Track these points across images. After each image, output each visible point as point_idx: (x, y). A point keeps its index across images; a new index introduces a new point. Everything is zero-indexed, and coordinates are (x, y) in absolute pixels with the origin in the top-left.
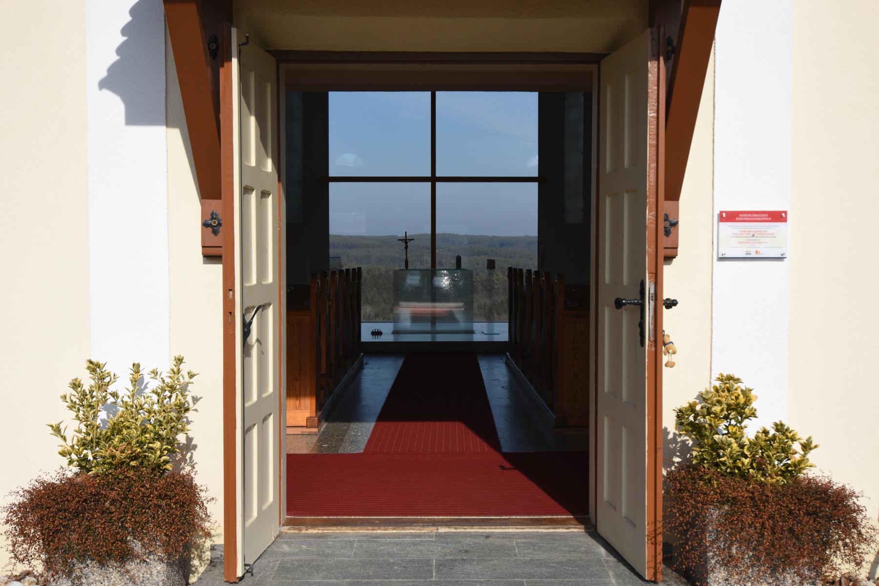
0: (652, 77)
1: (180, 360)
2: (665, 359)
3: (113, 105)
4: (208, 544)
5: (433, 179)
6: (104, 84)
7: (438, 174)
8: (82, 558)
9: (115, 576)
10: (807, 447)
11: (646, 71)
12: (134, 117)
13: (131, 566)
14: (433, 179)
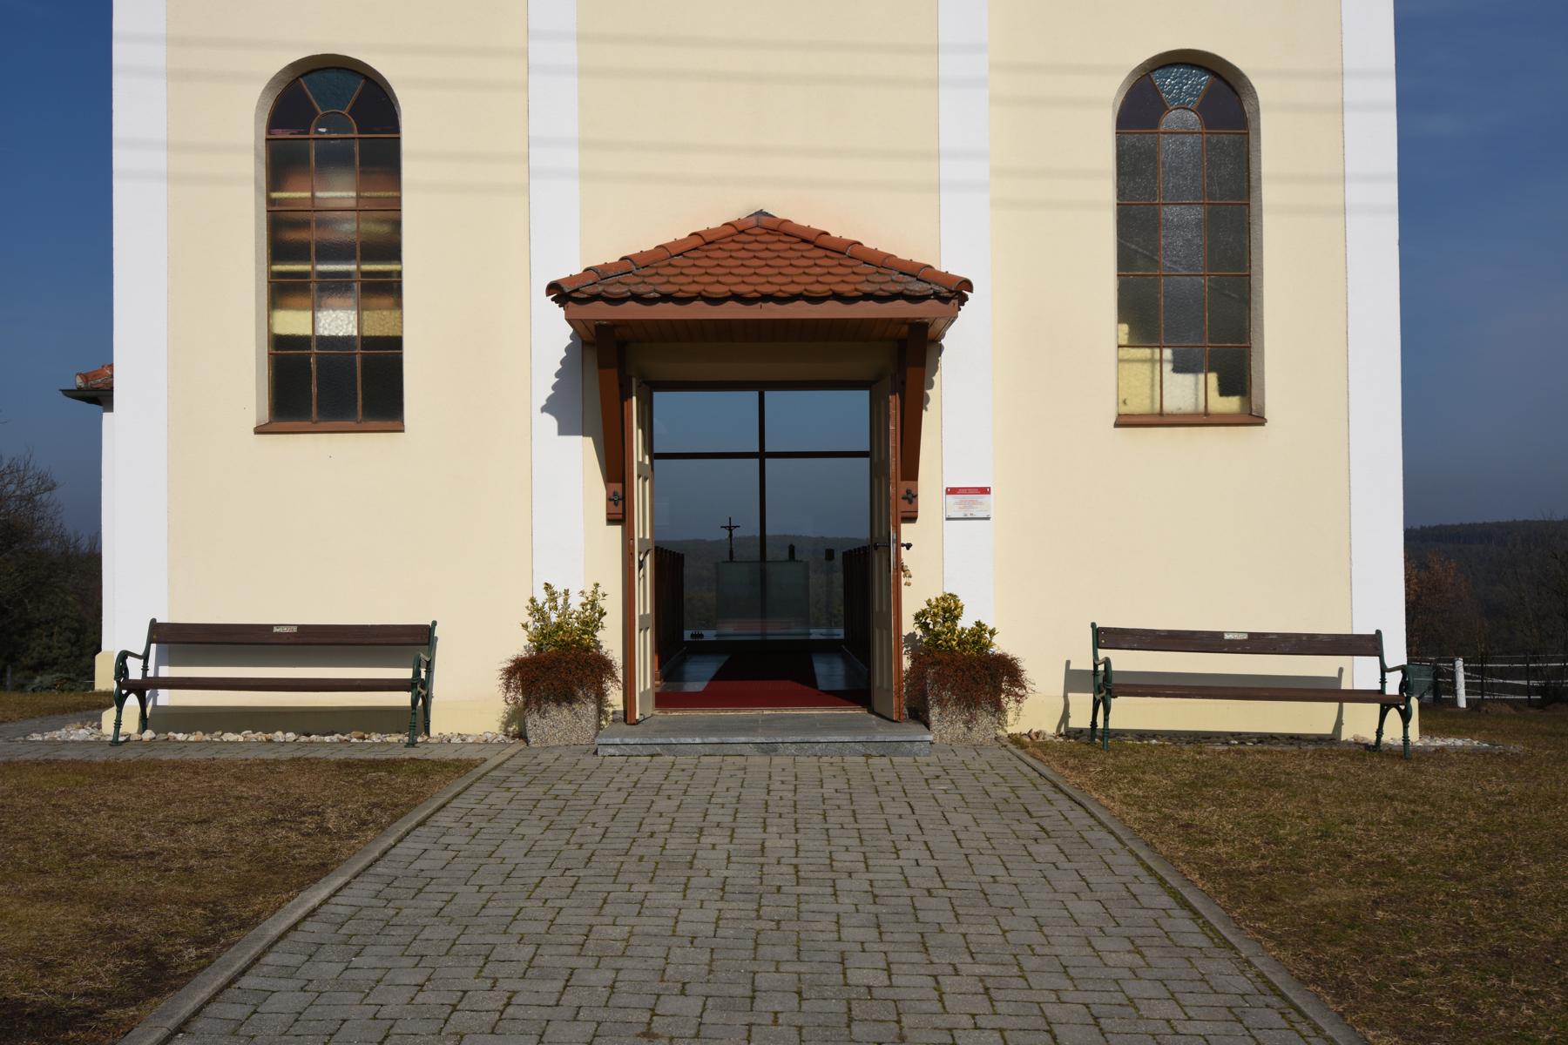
0: (892, 405)
2: (904, 580)
3: (551, 422)
4: (611, 710)
5: (762, 455)
6: (544, 409)
7: (756, 461)
8: (547, 700)
9: (566, 712)
10: (992, 633)
12: (564, 430)
13: (576, 706)
14: (762, 455)
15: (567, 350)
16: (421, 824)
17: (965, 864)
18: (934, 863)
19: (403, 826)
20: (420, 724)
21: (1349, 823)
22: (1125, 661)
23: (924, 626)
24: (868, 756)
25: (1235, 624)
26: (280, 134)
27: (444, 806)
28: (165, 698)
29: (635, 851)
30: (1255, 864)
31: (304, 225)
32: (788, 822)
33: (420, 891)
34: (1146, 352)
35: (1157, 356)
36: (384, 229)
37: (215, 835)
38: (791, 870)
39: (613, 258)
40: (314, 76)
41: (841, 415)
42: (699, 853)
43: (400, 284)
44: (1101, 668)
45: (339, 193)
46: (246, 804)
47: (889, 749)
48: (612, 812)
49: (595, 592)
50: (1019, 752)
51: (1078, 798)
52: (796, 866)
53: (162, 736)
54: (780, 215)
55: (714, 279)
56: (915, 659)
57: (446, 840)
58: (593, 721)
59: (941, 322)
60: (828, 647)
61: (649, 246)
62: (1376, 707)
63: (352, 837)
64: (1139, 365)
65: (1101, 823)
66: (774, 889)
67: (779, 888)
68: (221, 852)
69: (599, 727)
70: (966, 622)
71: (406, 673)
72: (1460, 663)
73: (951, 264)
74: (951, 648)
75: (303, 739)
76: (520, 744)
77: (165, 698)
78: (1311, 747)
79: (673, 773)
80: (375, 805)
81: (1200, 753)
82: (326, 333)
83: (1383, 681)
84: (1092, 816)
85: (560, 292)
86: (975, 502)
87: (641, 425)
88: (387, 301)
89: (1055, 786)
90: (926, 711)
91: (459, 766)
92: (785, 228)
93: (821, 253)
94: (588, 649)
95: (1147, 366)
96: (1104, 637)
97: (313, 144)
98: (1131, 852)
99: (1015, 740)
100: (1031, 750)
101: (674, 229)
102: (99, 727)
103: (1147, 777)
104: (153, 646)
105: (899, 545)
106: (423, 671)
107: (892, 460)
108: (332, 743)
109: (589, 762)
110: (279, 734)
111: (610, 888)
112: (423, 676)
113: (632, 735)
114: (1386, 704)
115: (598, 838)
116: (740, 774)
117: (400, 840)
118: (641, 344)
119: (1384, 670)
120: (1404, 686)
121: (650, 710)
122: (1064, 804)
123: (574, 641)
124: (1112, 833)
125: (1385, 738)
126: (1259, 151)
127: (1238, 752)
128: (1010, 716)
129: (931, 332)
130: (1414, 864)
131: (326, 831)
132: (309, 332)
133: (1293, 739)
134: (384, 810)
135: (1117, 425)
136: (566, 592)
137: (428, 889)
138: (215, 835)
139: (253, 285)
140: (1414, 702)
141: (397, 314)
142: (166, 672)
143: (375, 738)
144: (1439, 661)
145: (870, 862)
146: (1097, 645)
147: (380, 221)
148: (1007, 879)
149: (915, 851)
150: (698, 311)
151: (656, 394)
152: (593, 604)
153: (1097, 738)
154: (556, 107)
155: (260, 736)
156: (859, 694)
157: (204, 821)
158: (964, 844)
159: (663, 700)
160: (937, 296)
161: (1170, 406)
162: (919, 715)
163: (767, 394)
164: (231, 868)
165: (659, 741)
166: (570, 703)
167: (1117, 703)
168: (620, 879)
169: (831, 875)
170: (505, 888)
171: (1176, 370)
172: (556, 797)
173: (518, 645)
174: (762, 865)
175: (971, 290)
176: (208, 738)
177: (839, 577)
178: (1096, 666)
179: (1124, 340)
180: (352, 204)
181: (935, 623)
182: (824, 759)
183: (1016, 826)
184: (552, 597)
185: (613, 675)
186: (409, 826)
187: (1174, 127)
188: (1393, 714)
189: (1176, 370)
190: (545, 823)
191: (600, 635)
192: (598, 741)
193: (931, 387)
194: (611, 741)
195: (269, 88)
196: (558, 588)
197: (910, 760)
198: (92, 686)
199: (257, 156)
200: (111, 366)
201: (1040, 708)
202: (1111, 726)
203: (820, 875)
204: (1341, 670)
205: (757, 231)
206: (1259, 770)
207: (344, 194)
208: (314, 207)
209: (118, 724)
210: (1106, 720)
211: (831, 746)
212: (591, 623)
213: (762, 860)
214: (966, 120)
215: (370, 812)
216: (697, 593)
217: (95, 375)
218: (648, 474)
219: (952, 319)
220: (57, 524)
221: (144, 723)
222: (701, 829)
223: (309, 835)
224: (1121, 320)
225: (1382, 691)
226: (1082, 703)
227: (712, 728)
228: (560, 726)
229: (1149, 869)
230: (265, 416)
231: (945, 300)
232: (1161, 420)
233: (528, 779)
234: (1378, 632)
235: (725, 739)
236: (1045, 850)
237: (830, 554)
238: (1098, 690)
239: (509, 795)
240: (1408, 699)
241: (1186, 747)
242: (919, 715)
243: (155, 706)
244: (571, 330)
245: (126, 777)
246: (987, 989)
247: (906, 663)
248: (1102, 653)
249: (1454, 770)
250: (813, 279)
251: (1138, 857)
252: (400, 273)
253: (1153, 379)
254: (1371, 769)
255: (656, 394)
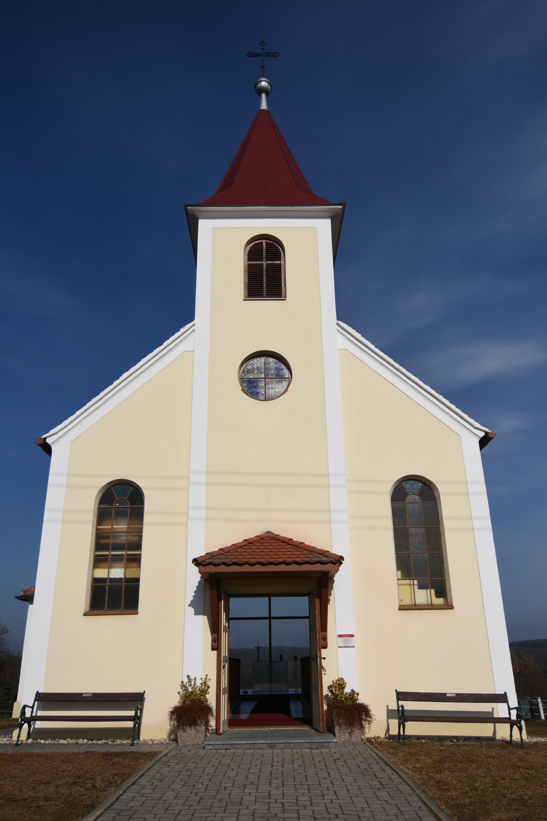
0: (317, 603)
1: (207, 675)
2: (323, 672)
3: (192, 610)
4: (211, 728)
5: (270, 618)
6: (189, 605)
9: (193, 730)
10: (358, 694)
11: (315, 601)
12: (196, 614)
13: (197, 727)
14: (270, 618)
15: (197, 587)
16: (133, 784)
17: (351, 801)
18: (338, 801)
19: (126, 785)
20: (136, 736)
21: (504, 779)
22: (409, 706)
23: (332, 692)
24: (311, 749)
25: (451, 690)
26: (103, 506)
27: (143, 775)
28: (39, 724)
29: (219, 796)
30: (467, 801)
31: (109, 537)
32: (279, 781)
33: (131, 817)
34: (407, 582)
35: (412, 583)
36: (136, 538)
37: (51, 789)
38: (281, 805)
39: (216, 549)
40: (116, 486)
41: (299, 605)
42: (244, 797)
43: (140, 559)
44: (400, 709)
45: (121, 526)
46: (65, 774)
47: (320, 745)
48: (210, 777)
49: (206, 678)
50: (370, 746)
51: (395, 769)
52: (283, 803)
53: (35, 741)
54: (276, 533)
55: (252, 557)
56: (328, 705)
57: (143, 791)
58: (204, 733)
59: (333, 572)
60: (295, 697)
61: (229, 544)
62: (508, 725)
63: (106, 790)
64: (406, 586)
65: (404, 781)
66: (274, 815)
67: (276, 814)
68: (53, 798)
69: (206, 736)
70: (347, 690)
71: (132, 713)
72: (539, 700)
73: (336, 551)
74: (342, 701)
75: (90, 742)
76: (174, 744)
77: (39, 724)
78: (485, 743)
79: (235, 758)
80: (116, 774)
81: (442, 746)
82: (113, 577)
83: (510, 714)
84: (401, 777)
85: (197, 562)
86: (348, 640)
87: (225, 611)
88: (135, 565)
89: (386, 763)
90: (334, 728)
91: (150, 755)
92: (277, 537)
93: (290, 546)
94: (203, 702)
95: (408, 587)
96: (401, 696)
97: (114, 509)
98: (417, 795)
99: (369, 740)
100: (375, 745)
101: (238, 539)
102: (12, 737)
103: (422, 758)
104: (36, 702)
105: (321, 658)
106: (139, 712)
107: (317, 624)
108: (101, 744)
109: (201, 752)
110: (81, 740)
111: (208, 815)
112: (139, 714)
113: (218, 740)
114: (512, 724)
115: (203, 790)
116: (261, 758)
117: (125, 792)
118: (225, 581)
119: (509, 709)
120: (518, 716)
121: (226, 728)
122: (389, 772)
123: (197, 699)
124: (409, 785)
125: (514, 738)
126: (441, 509)
127: (457, 745)
128: (367, 730)
129: (330, 575)
130: (531, 799)
131: (95, 787)
132: (106, 577)
133: (478, 739)
134: (119, 777)
135: (399, 609)
136: (195, 678)
137: (134, 816)
138: (51, 789)
139: (91, 532)
140: (523, 722)
141: (139, 569)
142: (40, 713)
143: (118, 742)
144: (531, 699)
145: (313, 801)
146: (398, 699)
147: (135, 536)
148: (368, 809)
149: (330, 796)
150: (246, 569)
151: (231, 599)
152: (205, 683)
153: (400, 739)
154: (198, 496)
155: (74, 741)
156: (307, 720)
157: (48, 783)
158: (350, 792)
159: (232, 723)
160: (331, 562)
161: (418, 602)
162: (331, 730)
163: (272, 598)
164: (56, 806)
165: (229, 743)
166: (195, 726)
167: (408, 724)
168: (212, 811)
169: (297, 808)
170: (165, 816)
171: (419, 588)
172: (188, 770)
173: (175, 701)
174: (269, 803)
175: (343, 560)
176: (53, 742)
177: (299, 667)
178: (398, 708)
179: (400, 577)
180: (125, 530)
181: (336, 690)
182: (294, 750)
183: (371, 783)
184: (190, 681)
185: (212, 714)
186: (128, 785)
187: (411, 501)
188: (515, 728)
189: (419, 588)
190: (183, 783)
191: (207, 696)
192: (206, 743)
193: (331, 595)
194: (210, 743)
195: (100, 490)
196: (192, 677)
197: (328, 750)
198: (11, 715)
199: (94, 514)
200: (34, 587)
201: (378, 726)
202: (406, 734)
203: (292, 808)
204: (493, 709)
205: (268, 538)
206: (465, 754)
207: (123, 527)
208: (112, 531)
209: (19, 736)
210: (404, 732)
211: (297, 745)
212: (204, 691)
213: (268, 800)
214: (339, 499)
215: (113, 778)
216: (245, 671)
217: (28, 590)
218: (227, 630)
219: (337, 570)
220: (7, 647)
221: (29, 735)
222: (245, 785)
223: (88, 789)
224: (398, 570)
225: (510, 718)
226: (394, 723)
227: (250, 736)
228: (191, 736)
229: (425, 803)
230: (88, 609)
231: (334, 564)
232: (415, 607)
233: (177, 761)
234: (505, 693)
235: (255, 742)
236: (383, 794)
237: (296, 658)
238: (400, 719)
239: (169, 769)
240: (520, 722)
241: (436, 743)
242: (331, 730)
243: (34, 728)
244: (200, 575)
245: (19, 761)
246: (374, 816)
247: (325, 707)
248: (401, 703)
249: (542, 753)
250: (287, 556)
251: (420, 797)
252: (140, 555)
253: (411, 592)
254: (509, 753)
255: (231, 599)
